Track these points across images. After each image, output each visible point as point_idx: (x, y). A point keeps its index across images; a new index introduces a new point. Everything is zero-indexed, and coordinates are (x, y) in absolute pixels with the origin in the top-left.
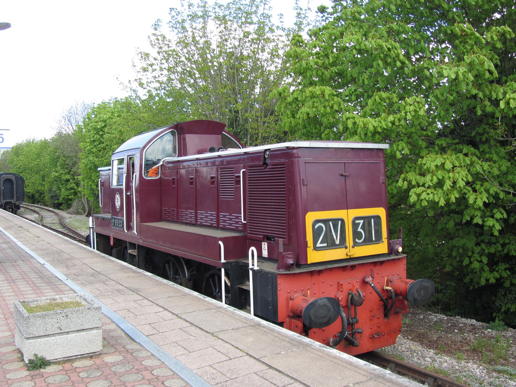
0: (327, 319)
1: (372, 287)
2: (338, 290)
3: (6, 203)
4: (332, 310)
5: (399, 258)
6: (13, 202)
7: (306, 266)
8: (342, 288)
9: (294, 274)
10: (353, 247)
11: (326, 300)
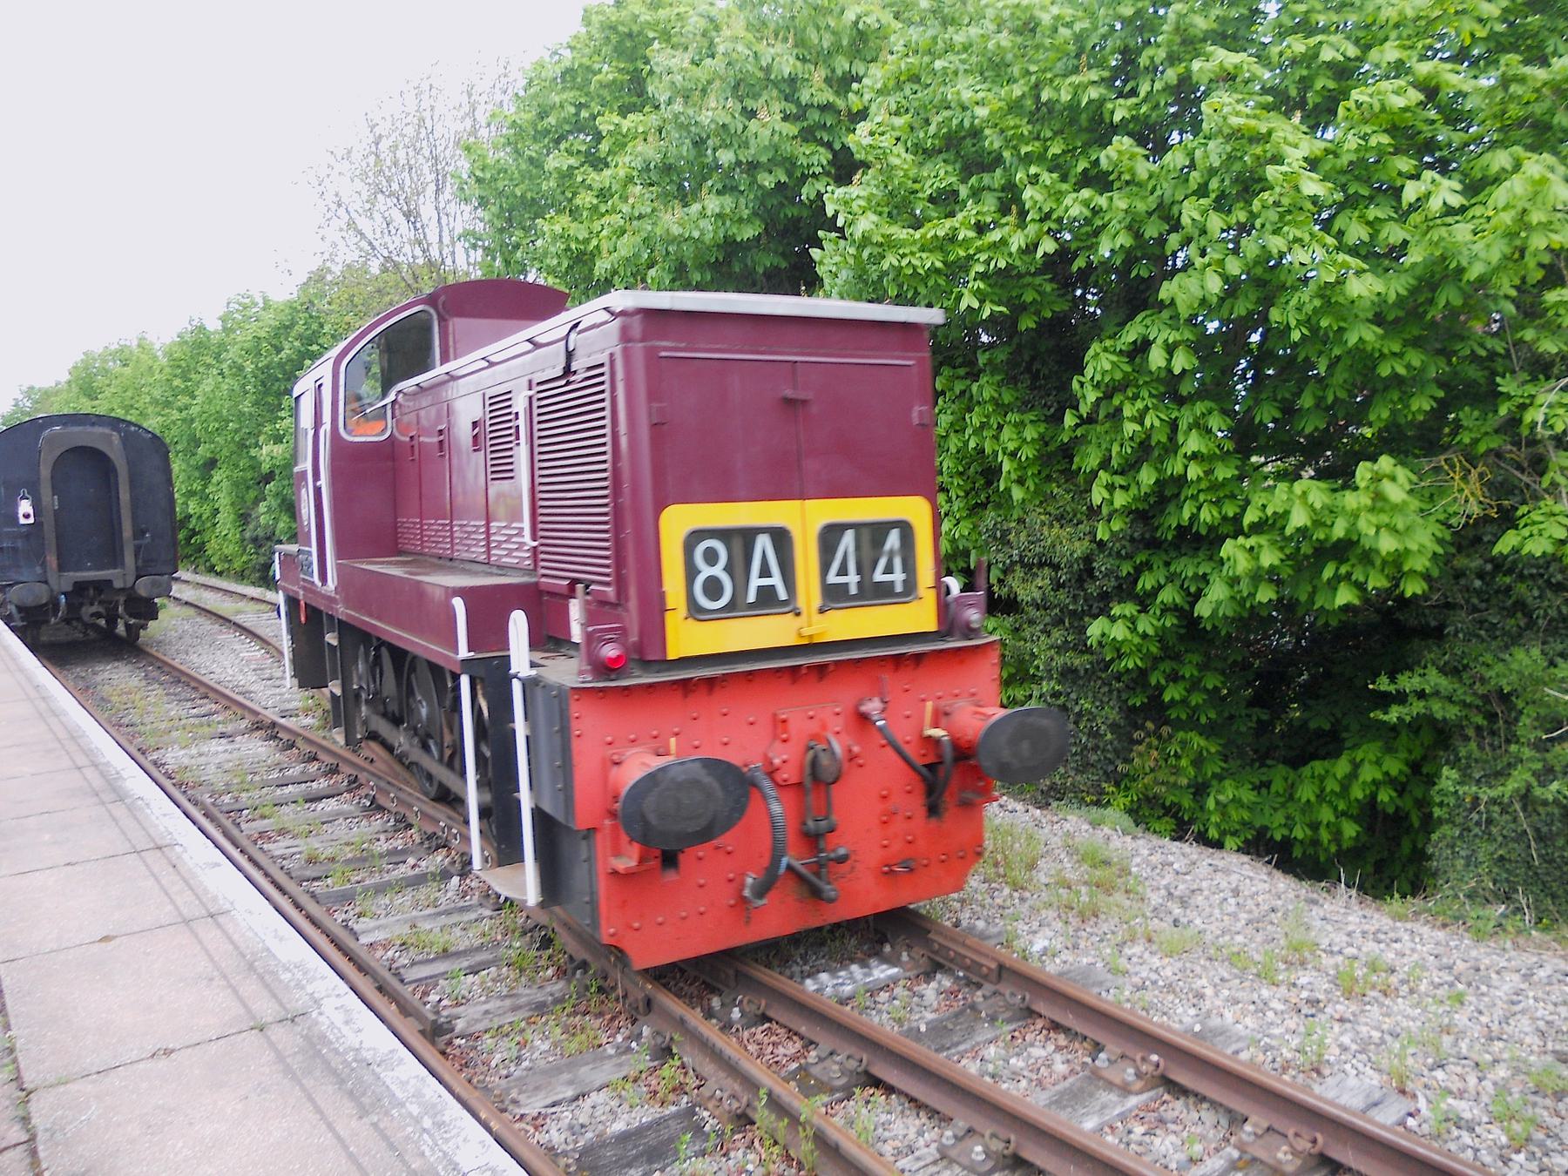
0: (703, 822)
1: (880, 729)
2: (775, 737)
3: (80, 588)
4: (720, 794)
5: (977, 647)
6: (118, 584)
7: (664, 666)
8: (785, 731)
9: (626, 688)
10: (822, 611)
11: (698, 765)
